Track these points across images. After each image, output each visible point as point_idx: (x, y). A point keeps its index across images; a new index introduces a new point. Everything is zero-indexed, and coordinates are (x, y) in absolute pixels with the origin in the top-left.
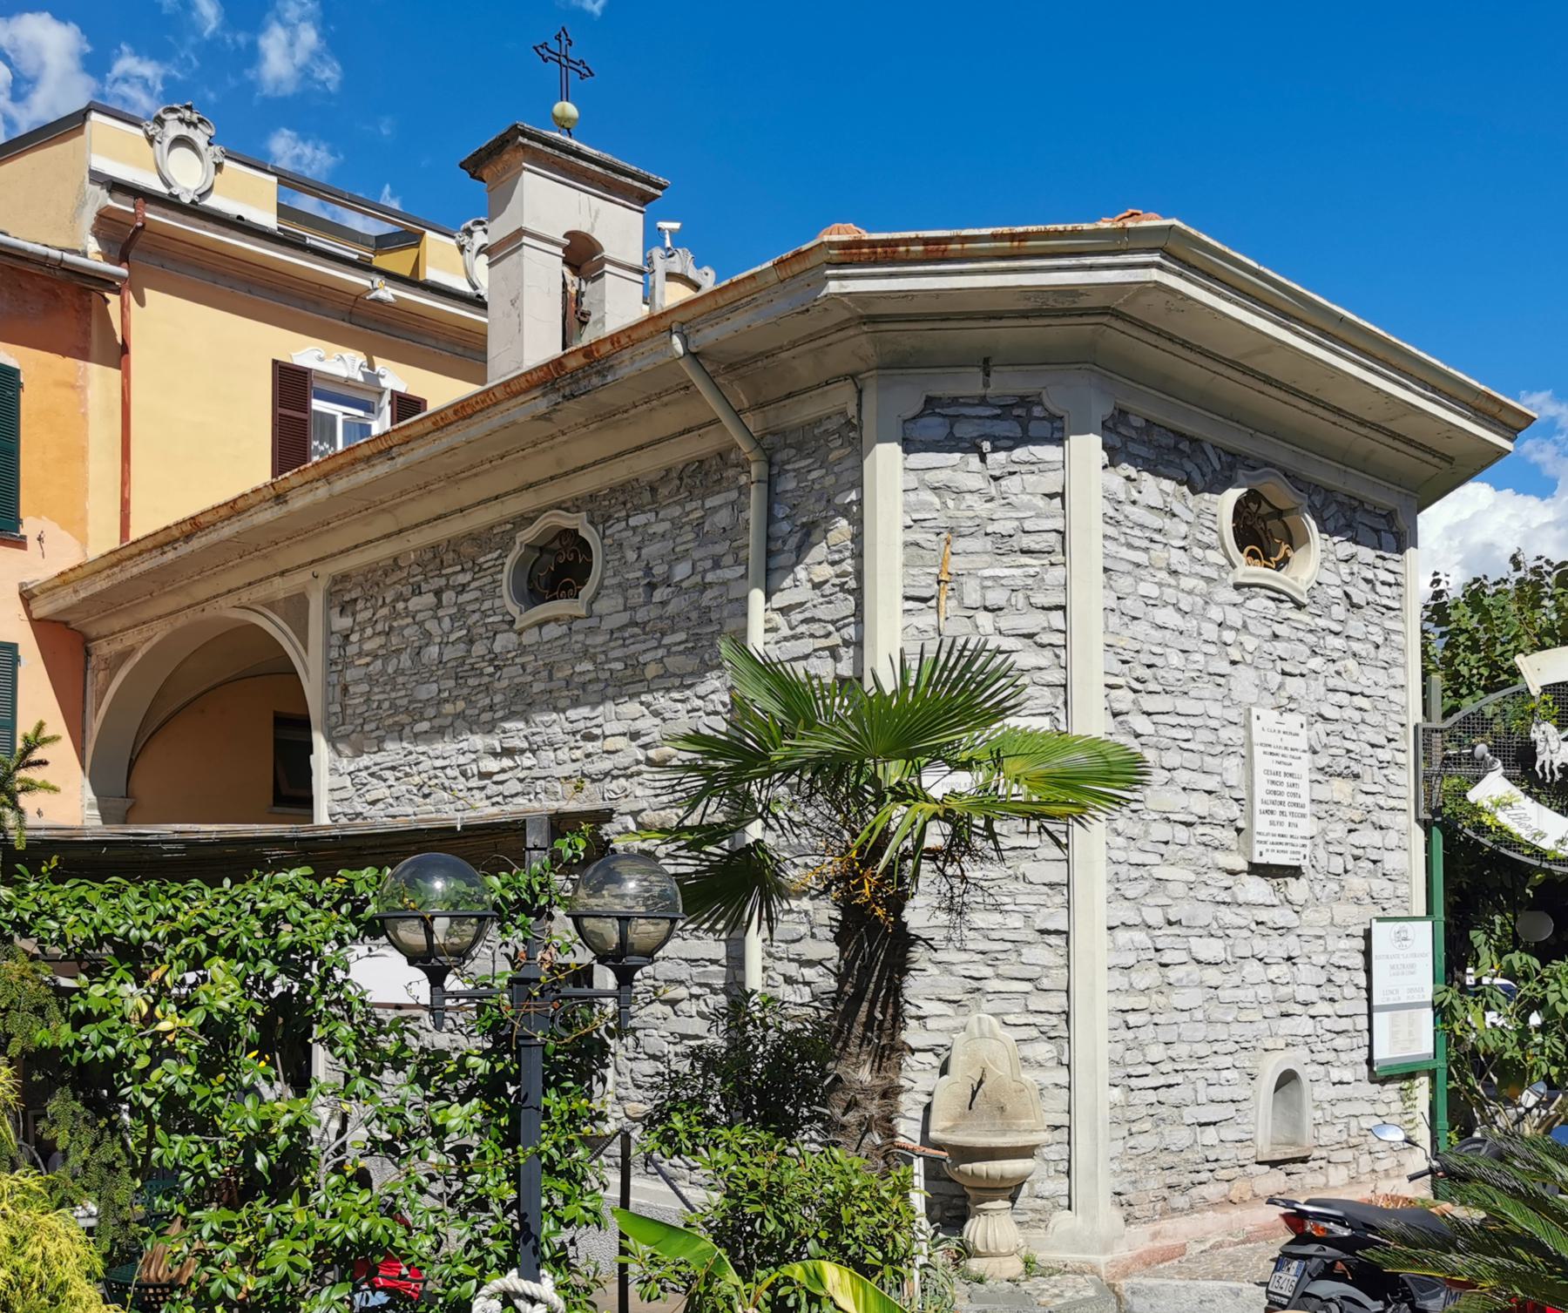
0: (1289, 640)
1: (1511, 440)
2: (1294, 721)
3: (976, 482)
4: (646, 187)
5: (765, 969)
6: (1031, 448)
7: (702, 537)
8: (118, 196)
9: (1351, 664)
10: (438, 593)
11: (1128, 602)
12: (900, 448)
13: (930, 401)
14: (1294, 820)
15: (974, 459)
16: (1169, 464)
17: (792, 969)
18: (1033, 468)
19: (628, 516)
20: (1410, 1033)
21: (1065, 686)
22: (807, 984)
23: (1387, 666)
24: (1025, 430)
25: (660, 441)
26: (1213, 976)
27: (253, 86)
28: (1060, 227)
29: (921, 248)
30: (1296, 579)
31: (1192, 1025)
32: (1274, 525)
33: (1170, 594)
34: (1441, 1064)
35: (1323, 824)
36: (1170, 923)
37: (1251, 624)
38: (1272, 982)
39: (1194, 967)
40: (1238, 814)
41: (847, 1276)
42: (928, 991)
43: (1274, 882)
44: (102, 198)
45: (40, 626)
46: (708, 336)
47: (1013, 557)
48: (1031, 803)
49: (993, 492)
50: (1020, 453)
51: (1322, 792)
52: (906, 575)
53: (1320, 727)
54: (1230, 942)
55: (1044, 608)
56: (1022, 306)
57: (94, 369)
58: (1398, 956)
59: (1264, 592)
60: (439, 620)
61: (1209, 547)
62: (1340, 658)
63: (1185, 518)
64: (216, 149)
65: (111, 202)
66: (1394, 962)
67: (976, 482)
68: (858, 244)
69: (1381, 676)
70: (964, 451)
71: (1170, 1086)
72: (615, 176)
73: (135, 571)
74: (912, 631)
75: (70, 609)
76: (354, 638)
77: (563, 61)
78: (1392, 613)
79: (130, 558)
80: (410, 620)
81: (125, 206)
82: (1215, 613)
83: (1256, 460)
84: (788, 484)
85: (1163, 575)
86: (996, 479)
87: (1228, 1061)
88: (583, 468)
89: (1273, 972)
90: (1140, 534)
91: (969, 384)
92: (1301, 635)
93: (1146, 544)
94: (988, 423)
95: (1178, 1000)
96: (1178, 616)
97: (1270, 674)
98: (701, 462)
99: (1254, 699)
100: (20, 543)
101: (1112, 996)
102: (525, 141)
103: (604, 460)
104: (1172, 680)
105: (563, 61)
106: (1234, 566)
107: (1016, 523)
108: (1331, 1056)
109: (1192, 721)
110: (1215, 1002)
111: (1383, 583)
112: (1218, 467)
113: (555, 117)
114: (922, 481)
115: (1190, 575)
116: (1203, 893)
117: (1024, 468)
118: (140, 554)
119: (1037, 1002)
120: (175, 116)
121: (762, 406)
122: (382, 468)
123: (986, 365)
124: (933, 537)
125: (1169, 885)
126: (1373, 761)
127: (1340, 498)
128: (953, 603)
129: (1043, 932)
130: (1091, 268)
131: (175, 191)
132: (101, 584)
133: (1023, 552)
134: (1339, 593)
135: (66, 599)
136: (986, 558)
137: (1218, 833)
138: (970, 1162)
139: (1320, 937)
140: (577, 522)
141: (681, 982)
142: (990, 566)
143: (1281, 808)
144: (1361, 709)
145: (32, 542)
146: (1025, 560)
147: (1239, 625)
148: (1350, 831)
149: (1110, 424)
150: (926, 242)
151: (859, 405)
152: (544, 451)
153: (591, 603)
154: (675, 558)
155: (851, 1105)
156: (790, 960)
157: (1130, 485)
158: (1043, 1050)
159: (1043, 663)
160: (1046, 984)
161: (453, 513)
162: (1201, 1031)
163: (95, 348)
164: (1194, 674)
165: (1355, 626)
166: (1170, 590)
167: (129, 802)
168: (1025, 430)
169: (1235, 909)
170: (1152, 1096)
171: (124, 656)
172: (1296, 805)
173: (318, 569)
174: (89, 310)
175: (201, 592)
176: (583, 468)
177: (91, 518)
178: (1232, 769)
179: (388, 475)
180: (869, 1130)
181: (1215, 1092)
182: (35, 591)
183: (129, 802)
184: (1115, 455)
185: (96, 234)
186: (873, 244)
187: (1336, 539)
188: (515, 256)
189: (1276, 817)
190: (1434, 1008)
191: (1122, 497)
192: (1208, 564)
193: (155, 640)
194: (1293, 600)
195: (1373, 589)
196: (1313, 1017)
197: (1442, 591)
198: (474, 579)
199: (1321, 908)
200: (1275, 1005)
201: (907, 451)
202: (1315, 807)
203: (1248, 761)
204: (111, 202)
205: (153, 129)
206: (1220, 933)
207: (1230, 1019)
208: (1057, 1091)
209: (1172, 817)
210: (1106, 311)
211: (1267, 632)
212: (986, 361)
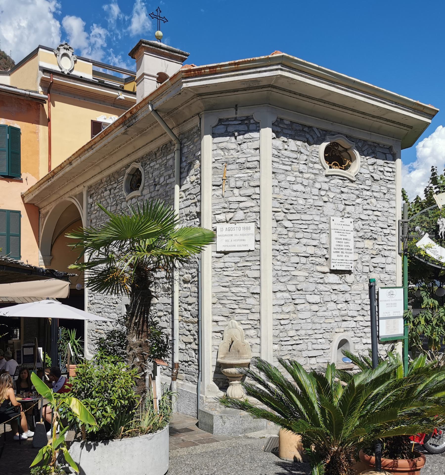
0: (348, 193)
1: (431, 119)
2: (347, 221)
3: (234, 146)
4: (182, 56)
5: (180, 306)
6: (250, 133)
7: (166, 169)
8: (45, 73)
9: (373, 200)
10: (110, 190)
11: (283, 183)
12: (211, 137)
13: (220, 120)
14: (347, 255)
15: (233, 138)
16: (300, 136)
17: (186, 306)
18: (251, 140)
19: (150, 163)
20: (394, 327)
21: (259, 212)
22: (189, 311)
23: (388, 200)
24: (248, 128)
25: (156, 139)
26: (315, 307)
27: (129, 33)
28: (249, 59)
29: (208, 70)
30: (350, 172)
31: (306, 324)
32: (344, 154)
33: (299, 180)
34: (406, 337)
35: (360, 256)
36: (298, 290)
37: (332, 189)
38: (339, 309)
39: (308, 305)
40: (326, 253)
41: (78, 402)
42: (219, 313)
43: (341, 276)
44: (42, 75)
45: (27, 205)
46: (158, 104)
47: (244, 170)
48: (174, 251)
49: (239, 149)
50: (247, 136)
51: (359, 245)
52: (213, 178)
53: (360, 222)
54: (322, 296)
55: (253, 187)
56: (243, 86)
57: (41, 127)
58: (389, 300)
59: (337, 177)
60: (110, 198)
61: (315, 163)
62: (368, 199)
63: (306, 154)
64: (74, 56)
65: (43, 76)
66: (388, 302)
67: (234, 146)
68: (190, 71)
69: (386, 204)
70: (230, 136)
71: (297, 344)
72: (172, 53)
73: (44, 187)
74: (215, 196)
75: (32, 200)
76: (93, 205)
77: (159, 18)
78: (391, 182)
79: (42, 184)
80: (104, 199)
81: (47, 76)
82: (318, 185)
83: (334, 132)
84: (185, 150)
85: (297, 174)
86: (240, 144)
87: (321, 336)
88: (139, 149)
89: (339, 306)
90: (288, 160)
91: (231, 114)
92: (352, 191)
93: (290, 163)
94: (237, 126)
95: (301, 316)
96: (303, 187)
97: (339, 205)
98: (166, 145)
99: (333, 214)
100: (21, 181)
101: (275, 315)
102: (144, 45)
103: (144, 146)
104: (300, 209)
105: (159, 18)
106: (325, 169)
107: (245, 159)
108: (363, 335)
109: (308, 222)
110: (316, 316)
111: (387, 172)
112: (319, 136)
113: (156, 36)
114: (218, 147)
115: (307, 173)
116: (311, 280)
117: (248, 140)
118: (44, 182)
119: (251, 317)
120: (62, 47)
121: (178, 125)
122: (91, 152)
123: (236, 107)
124: (221, 165)
125: (298, 277)
126: (382, 234)
127: (369, 143)
128: (227, 186)
129: (253, 293)
130: (260, 72)
131: (63, 70)
132: (37, 192)
133: (248, 168)
134: (369, 176)
135: (31, 197)
136: (237, 171)
137: (318, 260)
138: (226, 368)
139: (359, 294)
140: (138, 166)
141: (162, 311)
142: (238, 173)
143: (342, 251)
144: (377, 216)
145: (24, 180)
146: (248, 171)
147: (327, 189)
148: (372, 258)
149: (276, 124)
150: (210, 68)
151: (200, 123)
152: (129, 144)
153: (142, 191)
154: (161, 175)
155: (131, 349)
156: (186, 303)
157: (284, 143)
158: (252, 332)
159: (253, 205)
160: (253, 310)
161: (112, 165)
162: (310, 326)
163: (41, 120)
164: (309, 206)
165: (375, 187)
166: (300, 178)
167: (51, 257)
168: (248, 128)
169: (324, 285)
170: (290, 348)
171: (47, 213)
172: (348, 249)
173: (85, 184)
174: (39, 109)
175: (62, 192)
176: (139, 149)
177: (40, 172)
178: (324, 238)
179: (93, 154)
180: (135, 357)
181: (315, 346)
182: (24, 195)
183: (51, 257)
184: (278, 134)
185: (41, 86)
186: (194, 70)
187: (368, 157)
188: (142, 82)
189: (340, 254)
190: (404, 318)
191: (281, 148)
192: (315, 169)
193: (53, 208)
194: (349, 179)
195: (383, 174)
196: (356, 321)
197: (435, 173)
198: (117, 186)
199: (360, 284)
200: (340, 317)
201: (213, 137)
202: (357, 250)
203: (329, 234)
204: (43, 76)
205: (57, 52)
206: (319, 293)
207: (322, 322)
208: (256, 346)
209: (299, 254)
210: (270, 86)
211: (339, 191)
212: (236, 106)
